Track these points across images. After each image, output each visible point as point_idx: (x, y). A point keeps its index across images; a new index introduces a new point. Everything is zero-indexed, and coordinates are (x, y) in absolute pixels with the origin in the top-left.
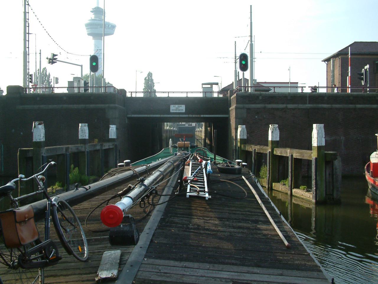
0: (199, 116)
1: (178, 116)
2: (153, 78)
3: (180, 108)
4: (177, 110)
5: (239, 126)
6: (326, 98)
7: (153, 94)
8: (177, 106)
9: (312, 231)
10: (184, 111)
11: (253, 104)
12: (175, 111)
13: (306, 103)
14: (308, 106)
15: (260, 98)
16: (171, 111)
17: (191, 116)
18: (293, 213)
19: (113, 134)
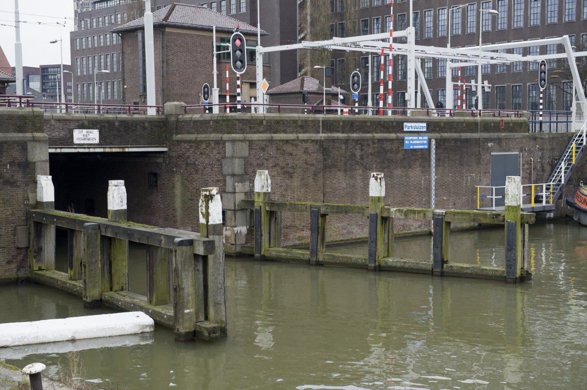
0: (121, 150)
1: (87, 150)
2: (37, 65)
3: (91, 136)
4: (85, 139)
5: (507, 177)
6: (511, 125)
7: (151, 98)
8: (85, 131)
9: (430, 303)
10: (97, 141)
11: (255, 133)
12: (82, 142)
13: (318, 132)
14: (322, 136)
15: (264, 123)
16: (76, 141)
17: (109, 151)
18: (69, 250)
19: (117, 201)
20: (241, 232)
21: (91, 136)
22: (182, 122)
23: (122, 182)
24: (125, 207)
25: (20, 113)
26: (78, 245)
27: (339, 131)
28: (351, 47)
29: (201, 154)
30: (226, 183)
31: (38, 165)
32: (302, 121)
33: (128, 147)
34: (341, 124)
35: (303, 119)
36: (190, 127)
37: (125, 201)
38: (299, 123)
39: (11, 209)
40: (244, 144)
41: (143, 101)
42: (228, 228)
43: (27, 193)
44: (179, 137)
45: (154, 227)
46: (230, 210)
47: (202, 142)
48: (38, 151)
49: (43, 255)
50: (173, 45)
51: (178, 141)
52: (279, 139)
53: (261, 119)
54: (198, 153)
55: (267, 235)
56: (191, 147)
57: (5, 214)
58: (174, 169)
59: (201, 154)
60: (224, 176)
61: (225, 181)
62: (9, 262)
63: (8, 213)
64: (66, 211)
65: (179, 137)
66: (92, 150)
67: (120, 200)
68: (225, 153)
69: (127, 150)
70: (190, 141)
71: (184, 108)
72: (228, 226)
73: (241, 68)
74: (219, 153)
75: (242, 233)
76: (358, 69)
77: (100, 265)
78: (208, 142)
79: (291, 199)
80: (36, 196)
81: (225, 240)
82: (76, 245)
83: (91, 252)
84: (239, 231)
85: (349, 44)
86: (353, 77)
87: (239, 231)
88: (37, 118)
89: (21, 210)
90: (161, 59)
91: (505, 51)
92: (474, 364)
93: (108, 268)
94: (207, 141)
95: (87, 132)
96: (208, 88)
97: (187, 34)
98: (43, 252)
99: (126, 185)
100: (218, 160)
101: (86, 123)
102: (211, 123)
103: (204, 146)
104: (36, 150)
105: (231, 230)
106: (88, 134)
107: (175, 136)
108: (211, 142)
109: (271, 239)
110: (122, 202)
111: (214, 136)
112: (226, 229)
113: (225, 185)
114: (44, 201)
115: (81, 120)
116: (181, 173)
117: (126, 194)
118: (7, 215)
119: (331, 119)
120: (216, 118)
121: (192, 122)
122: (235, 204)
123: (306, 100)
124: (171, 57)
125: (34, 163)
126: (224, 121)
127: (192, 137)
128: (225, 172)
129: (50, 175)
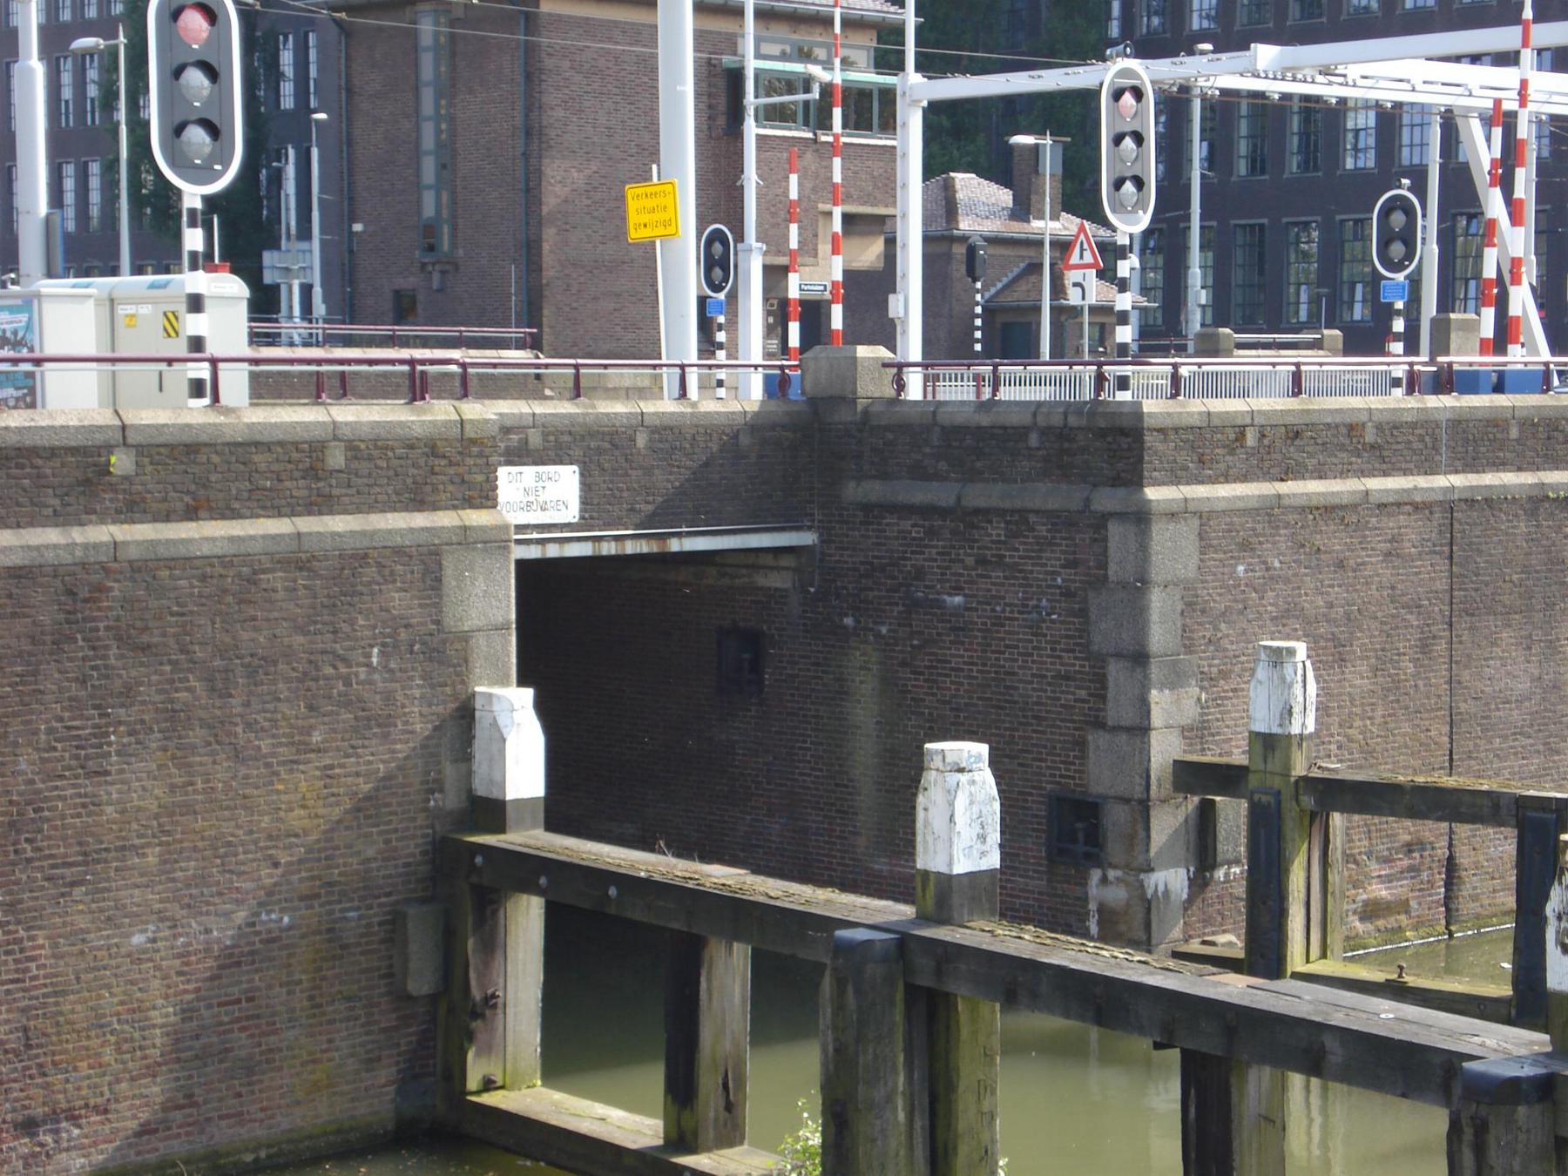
3: (551, 492)
8: (529, 471)
10: (572, 514)
15: (1251, 439)
17: (613, 552)
20: (1167, 892)
21: (551, 492)
22: (887, 428)
23: (983, 749)
24: (993, 860)
25: (418, 431)
26: (715, 1003)
27: (1504, 464)
28: (1313, 82)
29: (982, 561)
30: (1104, 687)
31: (480, 644)
32: (1379, 427)
33: (679, 535)
34: (1514, 433)
35: (1387, 417)
36: (928, 450)
37: (995, 837)
38: (1370, 436)
39: (380, 833)
40: (1182, 527)
41: (435, 285)
42: (1112, 874)
43: (439, 763)
44: (873, 490)
45: (1215, 970)
46: (1127, 801)
47: (985, 513)
48: (481, 584)
49: (501, 1028)
50: (566, 64)
51: (867, 508)
52: (1303, 501)
53: (1239, 422)
54: (970, 561)
55: (1303, 911)
56: (931, 533)
57: (359, 853)
58: (848, 621)
59: (982, 561)
60: (1099, 661)
61: (1101, 680)
62: (371, 1063)
63: (370, 852)
64: (652, 850)
65: (873, 490)
66: (553, 551)
67: (978, 829)
68: (1103, 565)
69: (675, 545)
70: (927, 511)
71: (895, 370)
72: (1115, 867)
73: (1134, 211)
74: (1072, 564)
75: (1173, 897)
76: (1406, 182)
77: (901, 1116)
78: (1018, 521)
79: (1340, 748)
80: (470, 774)
81: (1099, 923)
82: (710, 999)
83: (870, 1057)
84: (1161, 888)
85: (1308, 72)
86: (1386, 212)
87: (1161, 888)
88: (475, 449)
89: (414, 837)
90: (519, 120)
91: (1547, 56)
92: (23, 837)
93: (927, 1123)
94: (1013, 512)
95: (539, 477)
96: (725, 243)
97: (616, 24)
98: (500, 1011)
99: (996, 763)
100: (1068, 594)
101: (535, 439)
102: (1034, 440)
103: (996, 531)
104: (473, 580)
105: (1127, 884)
106: (541, 484)
107: (852, 484)
108: (1032, 518)
109: (1312, 924)
110: (982, 838)
111: (1047, 496)
112: (1104, 880)
113: (1103, 698)
114: (510, 796)
115: (520, 429)
116: (878, 635)
117: (997, 806)
118: (368, 860)
119: (1479, 415)
120: (1057, 420)
121: (937, 429)
122: (1148, 777)
123: (978, 272)
124: (560, 113)
125: (465, 637)
126: (1102, 433)
127: (940, 494)
128: (1098, 643)
129: (523, 681)
